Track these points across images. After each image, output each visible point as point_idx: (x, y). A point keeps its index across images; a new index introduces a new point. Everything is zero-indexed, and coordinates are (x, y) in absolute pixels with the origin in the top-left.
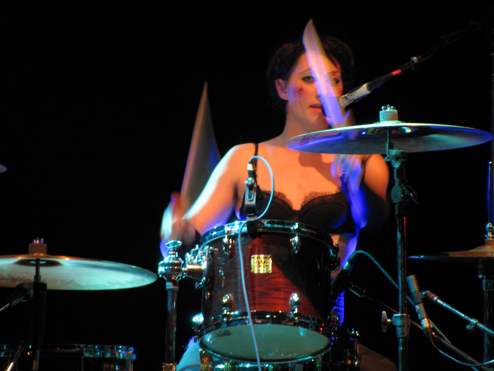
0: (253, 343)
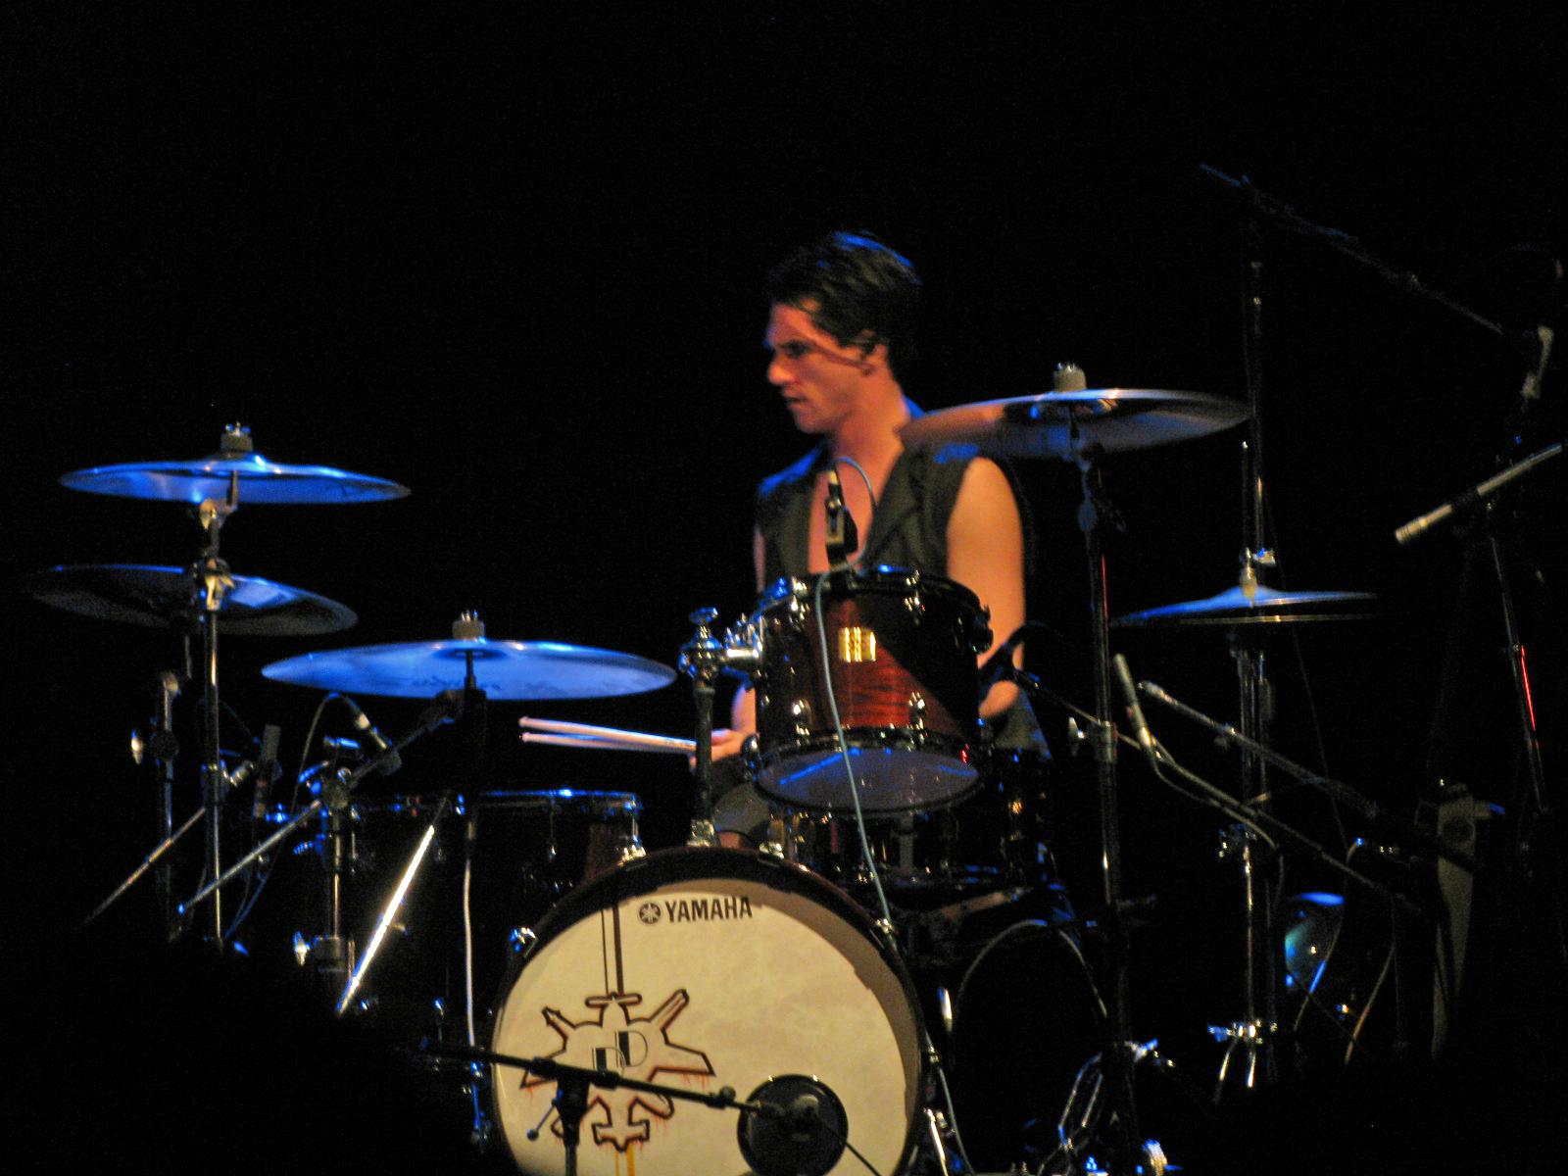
0: (850, 784)
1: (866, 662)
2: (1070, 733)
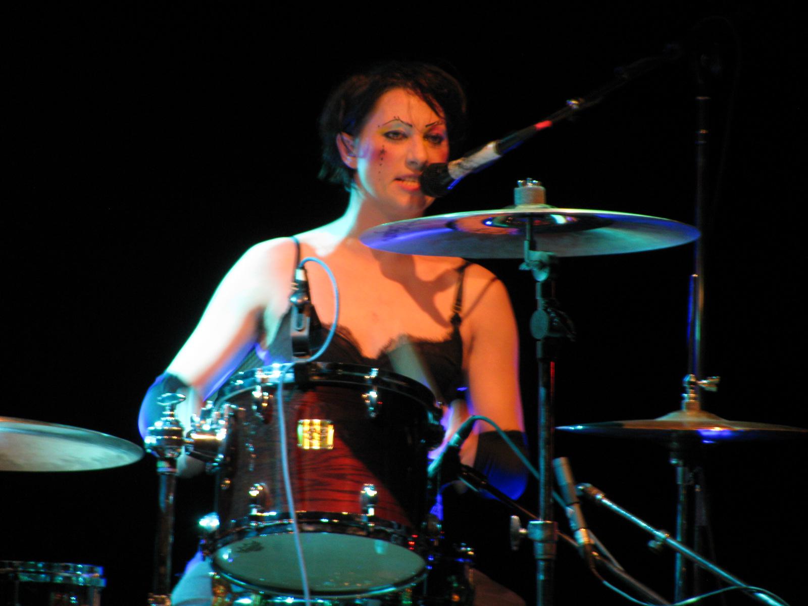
1: (323, 452)
2: (512, 530)
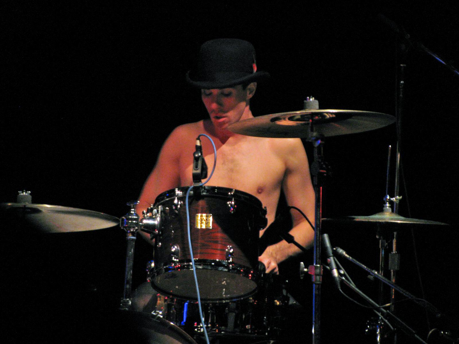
1: (207, 229)
2: (300, 269)
